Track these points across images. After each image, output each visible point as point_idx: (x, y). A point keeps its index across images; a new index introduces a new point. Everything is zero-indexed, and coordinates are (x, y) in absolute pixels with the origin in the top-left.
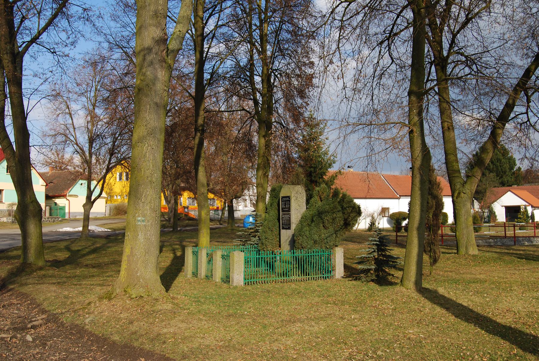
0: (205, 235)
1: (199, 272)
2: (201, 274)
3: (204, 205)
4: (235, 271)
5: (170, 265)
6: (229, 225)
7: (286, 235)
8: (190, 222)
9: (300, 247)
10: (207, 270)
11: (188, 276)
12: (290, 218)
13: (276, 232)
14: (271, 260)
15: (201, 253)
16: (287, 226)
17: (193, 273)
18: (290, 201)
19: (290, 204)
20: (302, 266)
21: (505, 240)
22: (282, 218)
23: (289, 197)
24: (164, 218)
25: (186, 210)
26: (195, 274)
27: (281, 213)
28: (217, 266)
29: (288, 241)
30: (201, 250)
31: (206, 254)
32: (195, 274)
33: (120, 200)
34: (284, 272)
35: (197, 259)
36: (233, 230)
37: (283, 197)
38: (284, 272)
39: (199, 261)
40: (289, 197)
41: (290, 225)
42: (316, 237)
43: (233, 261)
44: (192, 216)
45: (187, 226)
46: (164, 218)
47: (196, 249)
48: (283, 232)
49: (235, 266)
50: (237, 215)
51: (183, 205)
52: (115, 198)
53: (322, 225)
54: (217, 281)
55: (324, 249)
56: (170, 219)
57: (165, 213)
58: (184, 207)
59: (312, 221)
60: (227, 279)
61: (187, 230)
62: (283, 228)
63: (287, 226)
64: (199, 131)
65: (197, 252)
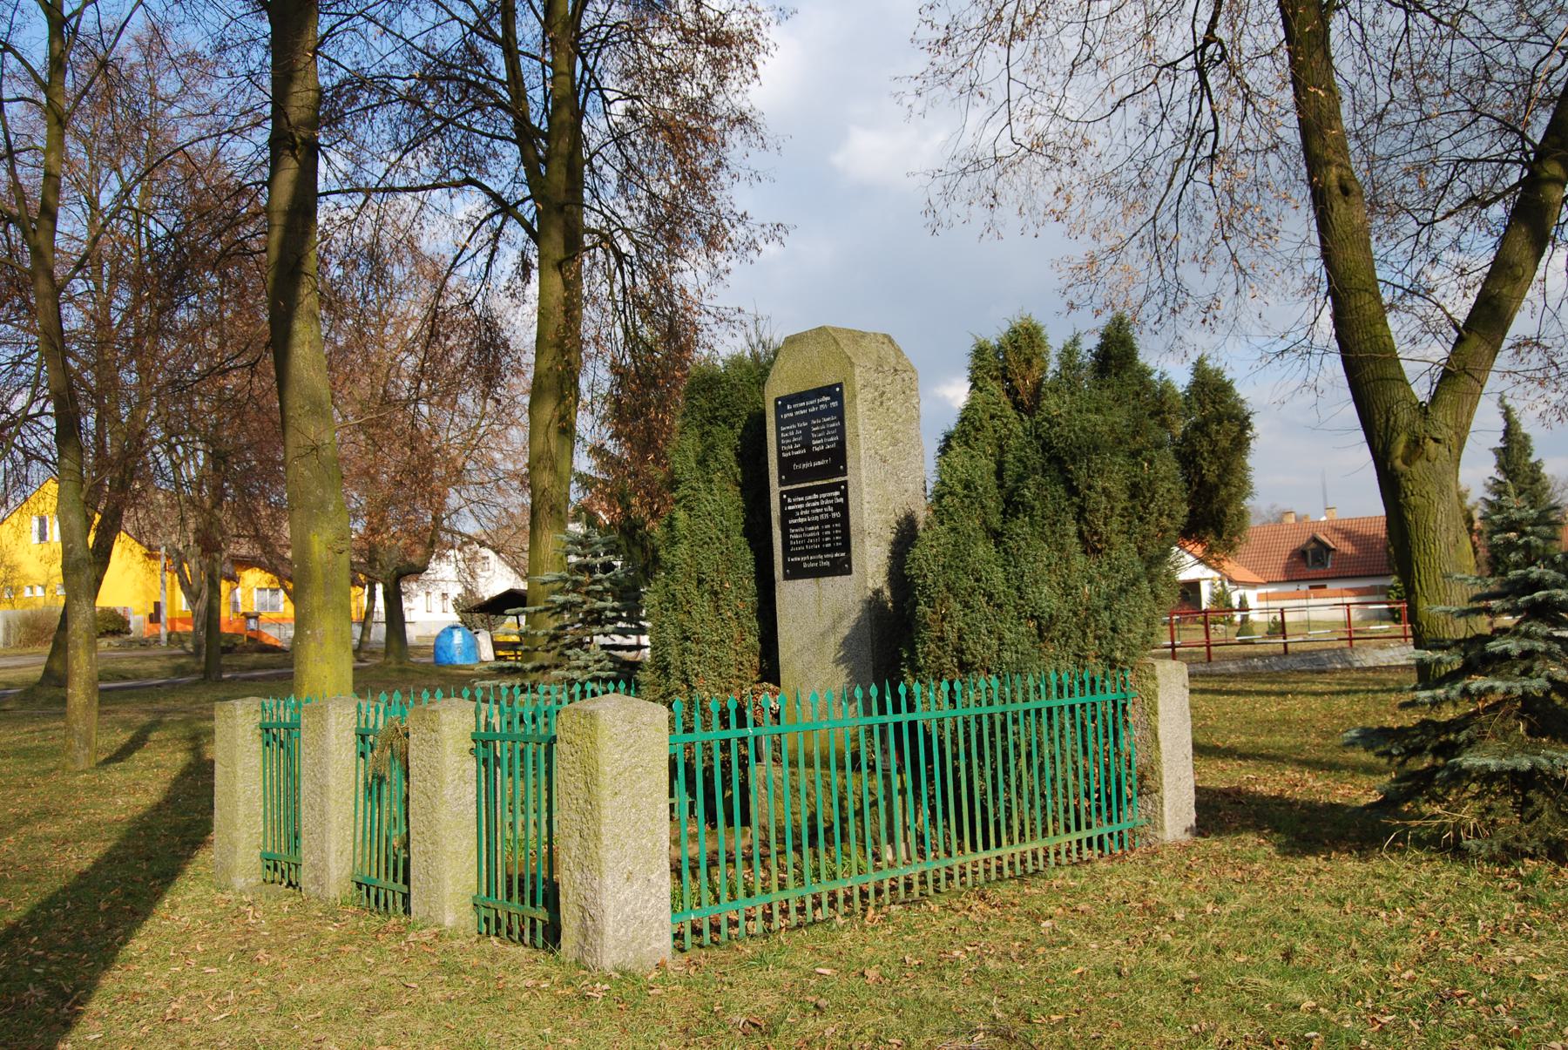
0: (329, 648)
1: (307, 857)
2: (321, 869)
3: (322, 505)
4: (609, 855)
5: (158, 808)
6: (392, 658)
7: (816, 614)
8: (265, 656)
9: (949, 662)
10: (373, 835)
11: (239, 882)
12: (843, 508)
13: (742, 597)
14: (718, 756)
15: (322, 734)
16: (829, 551)
17: (265, 857)
18: (840, 413)
19: (841, 431)
20: (959, 790)
21: (1289, 660)
22: (786, 515)
23: (834, 392)
24: (183, 648)
25: (252, 623)
26: (282, 868)
27: (775, 490)
28: (444, 814)
29: (834, 641)
30: (320, 712)
31: (351, 737)
32: (282, 868)
33: (41, 602)
34: (813, 818)
35: (293, 777)
36: (403, 671)
37: (783, 403)
38: (813, 818)
39: (305, 786)
40: (834, 392)
41: (846, 546)
42: (1047, 598)
43: (591, 781)
44: (271, 642)
45: (254, 668)
46: (183, 648)
47: (282, 711)
48: (793, 597)
49: (607, 813)
50: (412, 633)
51: (242, 609)
52: (27, 593)
53: (1072, 529)
54: (449, 920)
55: (1096, 668)
56: (198, 647)
57: (187, 634)
58: (248, 616)
59: (1012, 506)
60: (533, 904)
61: (253, 679)
62: (794, 572)
63: (829, 551)
64: (293, 148)
65: (292, 727)
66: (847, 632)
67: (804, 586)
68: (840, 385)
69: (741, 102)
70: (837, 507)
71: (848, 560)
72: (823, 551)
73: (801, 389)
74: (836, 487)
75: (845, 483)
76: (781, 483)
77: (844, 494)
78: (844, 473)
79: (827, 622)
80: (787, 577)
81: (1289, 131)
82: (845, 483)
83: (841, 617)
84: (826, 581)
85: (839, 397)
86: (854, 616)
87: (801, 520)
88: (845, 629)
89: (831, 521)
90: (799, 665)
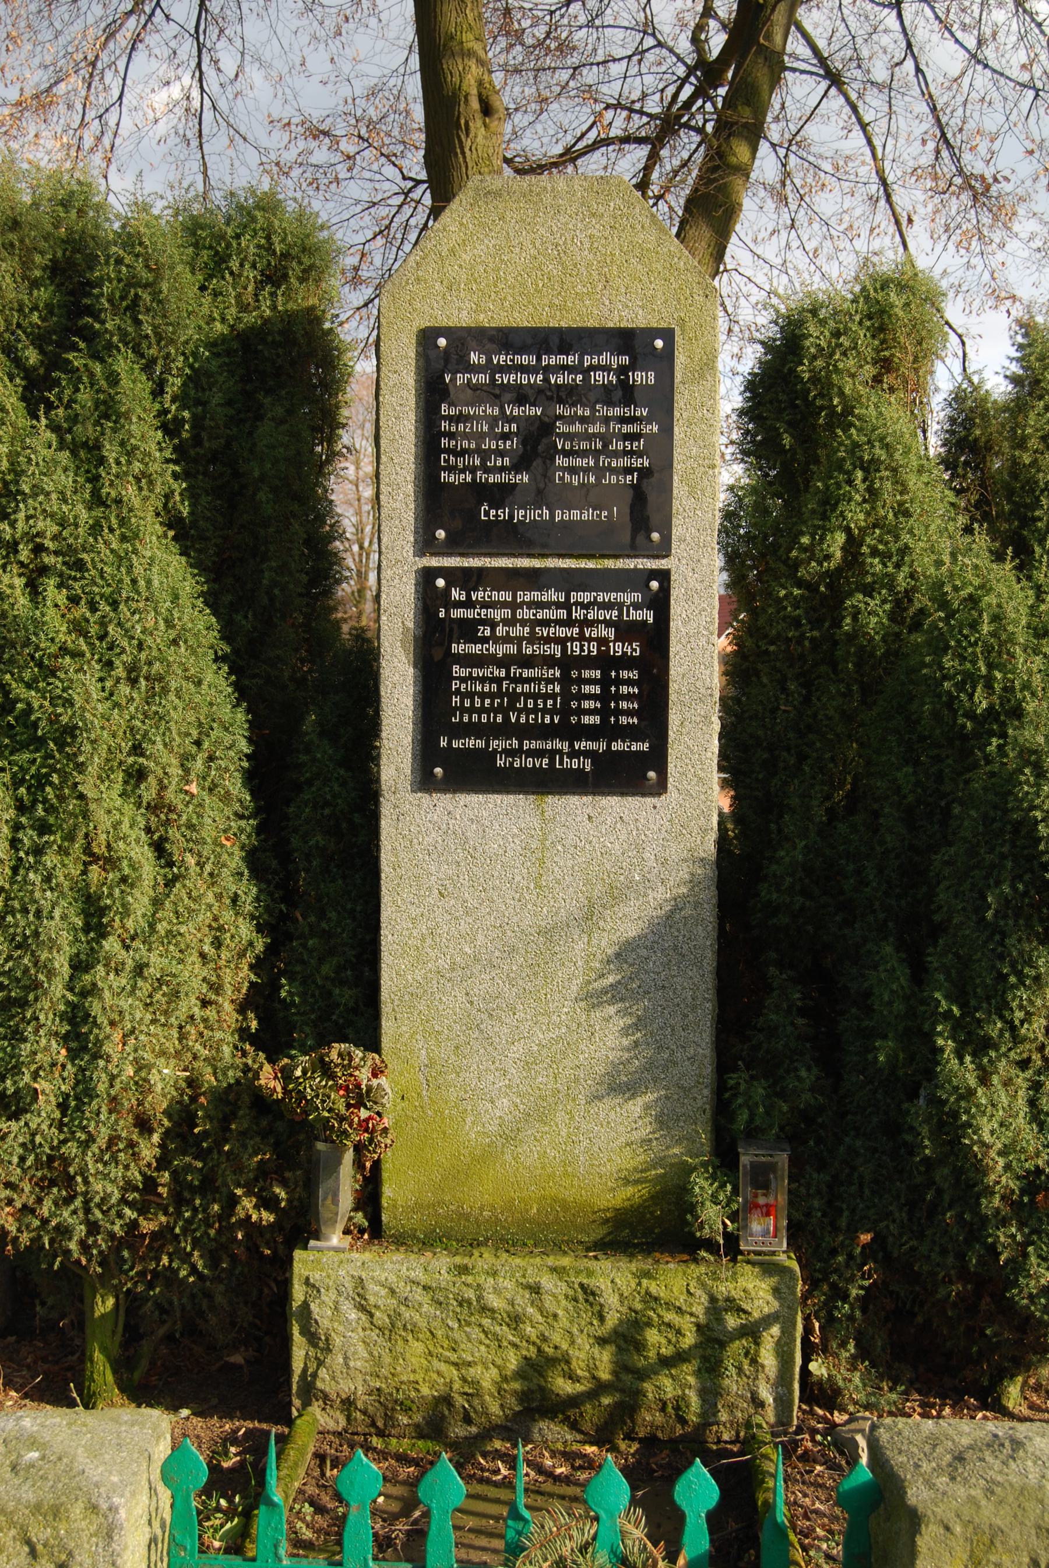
29: (584, 957)
66: (631, 930)
67: (495, 820)
68: (668, 335)
69: (636, 1107)
70: (626, 631)
71: (658, 758)
72: (572, 732)
73: (521, 318)
74: (637, 580)
75: (420, 552)
76: (425, 544)
77: (660, 603)
78: (664, 550)
79: (568, 901)
80: (425, 782)
81: (384, 618)
82: (664, 576)
83: (616, 895)
84: (573, 808)
85: (665, 361)
86: (659, 898)
87: (500, 650)
88: (628, 922)
89: (605, 661)
90: (453, 1001)
